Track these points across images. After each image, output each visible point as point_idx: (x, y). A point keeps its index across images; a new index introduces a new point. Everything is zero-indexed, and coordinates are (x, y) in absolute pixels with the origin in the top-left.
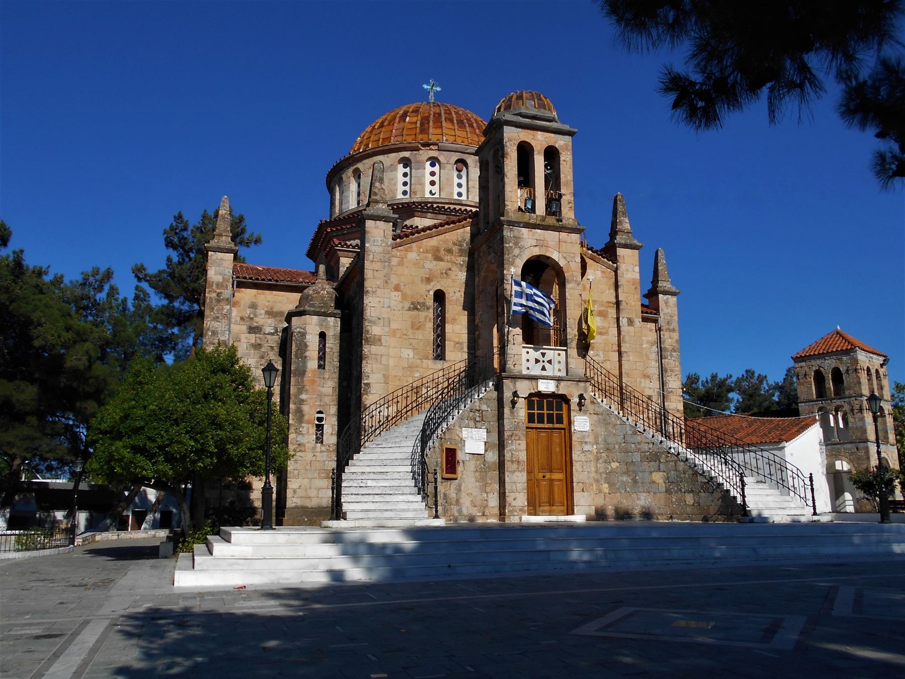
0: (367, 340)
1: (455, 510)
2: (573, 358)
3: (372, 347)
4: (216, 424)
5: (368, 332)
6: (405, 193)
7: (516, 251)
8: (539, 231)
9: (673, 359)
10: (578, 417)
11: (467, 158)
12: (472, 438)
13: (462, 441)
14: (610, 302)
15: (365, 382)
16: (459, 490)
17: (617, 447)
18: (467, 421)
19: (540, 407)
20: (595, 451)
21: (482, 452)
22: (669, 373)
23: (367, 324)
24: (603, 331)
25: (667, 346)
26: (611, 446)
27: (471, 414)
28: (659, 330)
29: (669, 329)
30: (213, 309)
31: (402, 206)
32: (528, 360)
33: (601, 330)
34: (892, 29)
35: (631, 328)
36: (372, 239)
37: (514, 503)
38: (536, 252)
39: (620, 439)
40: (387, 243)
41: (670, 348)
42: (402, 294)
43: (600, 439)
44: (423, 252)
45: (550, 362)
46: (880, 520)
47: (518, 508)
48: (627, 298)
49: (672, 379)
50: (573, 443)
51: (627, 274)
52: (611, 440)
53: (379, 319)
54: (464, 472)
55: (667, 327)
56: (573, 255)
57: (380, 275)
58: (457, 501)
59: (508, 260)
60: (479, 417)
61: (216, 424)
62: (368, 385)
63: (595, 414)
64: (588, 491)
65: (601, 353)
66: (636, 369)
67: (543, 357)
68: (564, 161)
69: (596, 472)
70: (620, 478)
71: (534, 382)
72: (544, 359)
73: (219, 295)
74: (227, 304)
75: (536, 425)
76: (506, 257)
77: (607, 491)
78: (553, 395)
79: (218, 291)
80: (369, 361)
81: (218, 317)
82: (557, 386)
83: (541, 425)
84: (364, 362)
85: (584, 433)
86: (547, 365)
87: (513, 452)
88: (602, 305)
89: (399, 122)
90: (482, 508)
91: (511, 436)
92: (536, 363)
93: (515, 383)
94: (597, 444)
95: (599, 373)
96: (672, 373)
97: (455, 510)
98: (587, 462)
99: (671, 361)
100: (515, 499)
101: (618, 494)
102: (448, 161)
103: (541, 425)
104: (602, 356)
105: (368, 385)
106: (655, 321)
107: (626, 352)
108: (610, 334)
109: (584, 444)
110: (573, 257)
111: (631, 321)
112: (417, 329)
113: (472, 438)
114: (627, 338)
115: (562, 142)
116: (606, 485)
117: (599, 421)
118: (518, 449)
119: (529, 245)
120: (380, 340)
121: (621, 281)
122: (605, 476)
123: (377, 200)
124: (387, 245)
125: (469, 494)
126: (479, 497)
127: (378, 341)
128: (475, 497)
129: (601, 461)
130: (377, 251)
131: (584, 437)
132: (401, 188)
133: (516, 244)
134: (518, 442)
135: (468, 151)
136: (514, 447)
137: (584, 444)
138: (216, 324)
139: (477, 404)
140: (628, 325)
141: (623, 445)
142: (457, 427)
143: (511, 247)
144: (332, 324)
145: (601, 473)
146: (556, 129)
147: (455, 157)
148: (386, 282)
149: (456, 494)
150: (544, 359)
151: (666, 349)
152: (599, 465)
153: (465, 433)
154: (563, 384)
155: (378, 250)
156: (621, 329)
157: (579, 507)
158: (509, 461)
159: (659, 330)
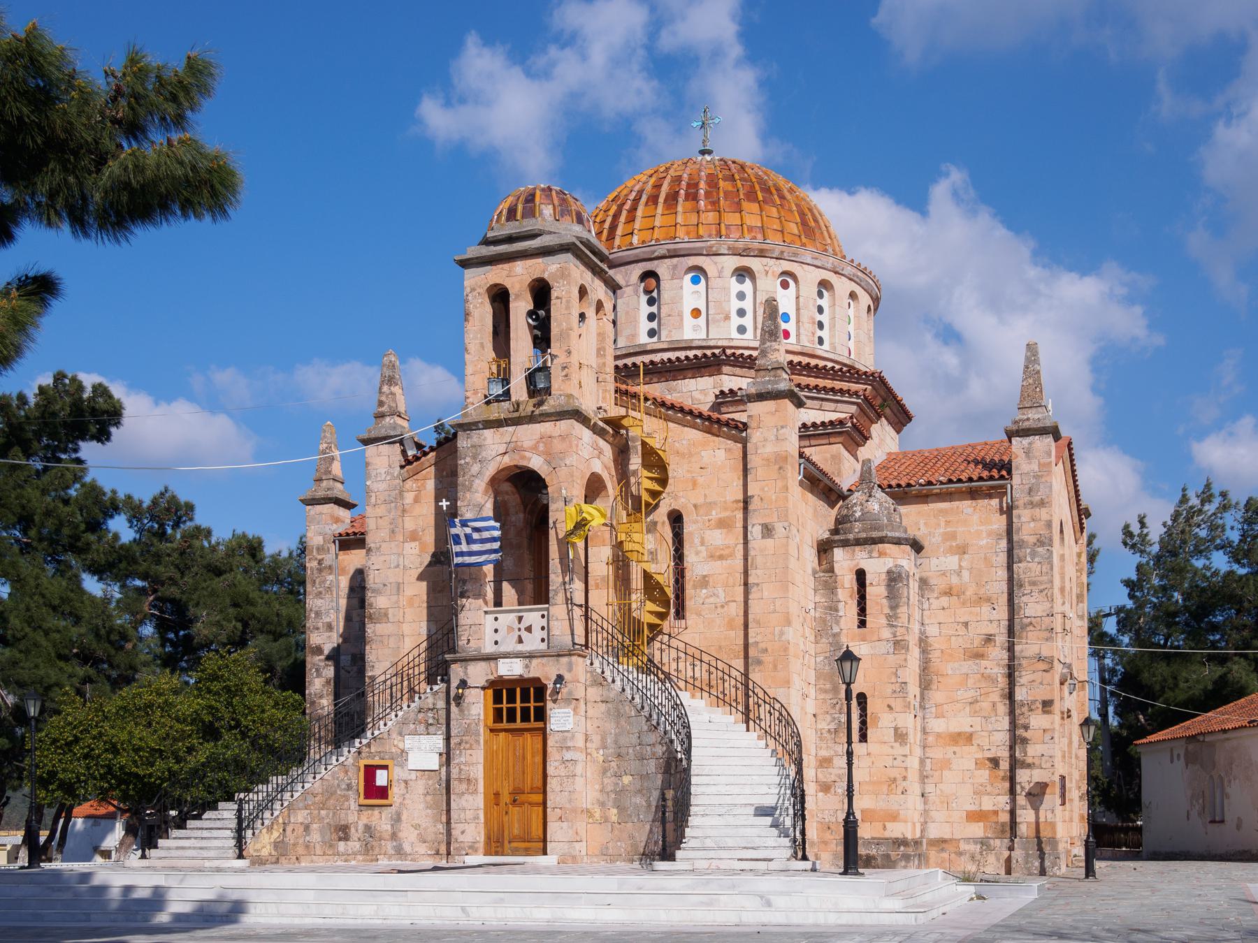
0: (370, 617)
1: (389, 848)
2: (557, 619)
3: (377, 625)
5: (371, 605)
6: (652, 333)
7: (475, 468)
9: (1036, 560)
10: (556, 711)
11: (657, 266)
12: (419, 749)
15: (370, 674)
16: (397, 819)
17: (631, 751)
18: (412, 726)
19: (511, 699)
20: (601, 759)
22: (1027, 589)
23: (369, 594)
24: (726, 552)
25: (1026, 538)
26: (623, 751)
27: (421, 716)
28: (1008, 511)
30: (314, 582)
32: (496, 631)
33: (722, 552)
34: (179, 213)
35: (769, 542)
36: (373, 474)
37: (461, 838)
38: (507, 461)
39: (634, 740)
40: (392, 474)
41: (1032, 539)
42: (420, 543)
43: (609, 741)
44: (447, 476)
45: (529, 629)
46: (842, 870)
47: (466, 844)
48: (763, 489)
49: (1032, 599)
50: (549, 749)
51: (763, 446)
52: (624, 741)
53: (385, 585)
54: (407, 796)
55: (1027, 498)
57: (384, 523)
58: (394, 836)
59: (463, 485)
60: (434, 718)
62: (373, 678)
63: (602, 702)
64: (568, 821)
65: (720, 591)
66: (774, 611)
68: (557, 298)
69: (601, 791)
70: (633, 800)
71: (492, 663)
73: (320, 562)
74: (330, 574)
75: (505, 725)
76: (460, 479)
77: (614, 819)
78: (521, 681)
79: (320, 557)
80: (374, 647)
81: (320, 593)
82: (527, 667)
83: (512, 726)
84: (367, 647)
85: (566, 734)
86: (524, 634)
87: (462, 767)
88: (726, 509)
89: (646, 204)
90: (436, 844)
91: (460, 744)
93: (466, 668)
94: (604, 747)
95: (610, 637)
96: (1033, 588)
97: (389, 848)
98: (568, 777)
99: (1034, 566)
100: (463, 832)
101: (630, 825)
102: (627, 282)
103: (512, 726)
104: (722, 595)
105: (373, 678)
107: (758, 584)
109: (564, 750)
111: (768, 530)
112: (439, 592)
113: (419, 749)
114: (759, 560)
115: (555, 266)
116: (615, 811)
117: (608, 711)
118: (473, 762)
119: (494, 453)
120: (386, 615)
121: (753, 460)
122: (613, 796)
123: (382, 412)
124: (394, 478)
125: (417, 827)
126: (431, 830)
127: (383, 617)
128: (425, 829)
129: (609, 774)
130: (381, 489)
131: (565, 739)
132: (645, 325)
133: (474, 457)
134: (469, 752)
135: (656, 254)
136: (463, 759)
137: (564, 750)
138: (319, 602)
139: (430, 700)
141: (638, 748)
142: (394, 735)
143: (467, 463)
145: (608, 793)
146: (537, 248)
147: (638, 269)
148: (393, 532)
149: (392, 825)
151: (1022, 544)
152: (606, 781)
153: (409, 742)
154: (535, 662)
155: (382, 486)
156: (750, 546)
157: (553, 844)
158: (455, 779)
159: (1008, 511)
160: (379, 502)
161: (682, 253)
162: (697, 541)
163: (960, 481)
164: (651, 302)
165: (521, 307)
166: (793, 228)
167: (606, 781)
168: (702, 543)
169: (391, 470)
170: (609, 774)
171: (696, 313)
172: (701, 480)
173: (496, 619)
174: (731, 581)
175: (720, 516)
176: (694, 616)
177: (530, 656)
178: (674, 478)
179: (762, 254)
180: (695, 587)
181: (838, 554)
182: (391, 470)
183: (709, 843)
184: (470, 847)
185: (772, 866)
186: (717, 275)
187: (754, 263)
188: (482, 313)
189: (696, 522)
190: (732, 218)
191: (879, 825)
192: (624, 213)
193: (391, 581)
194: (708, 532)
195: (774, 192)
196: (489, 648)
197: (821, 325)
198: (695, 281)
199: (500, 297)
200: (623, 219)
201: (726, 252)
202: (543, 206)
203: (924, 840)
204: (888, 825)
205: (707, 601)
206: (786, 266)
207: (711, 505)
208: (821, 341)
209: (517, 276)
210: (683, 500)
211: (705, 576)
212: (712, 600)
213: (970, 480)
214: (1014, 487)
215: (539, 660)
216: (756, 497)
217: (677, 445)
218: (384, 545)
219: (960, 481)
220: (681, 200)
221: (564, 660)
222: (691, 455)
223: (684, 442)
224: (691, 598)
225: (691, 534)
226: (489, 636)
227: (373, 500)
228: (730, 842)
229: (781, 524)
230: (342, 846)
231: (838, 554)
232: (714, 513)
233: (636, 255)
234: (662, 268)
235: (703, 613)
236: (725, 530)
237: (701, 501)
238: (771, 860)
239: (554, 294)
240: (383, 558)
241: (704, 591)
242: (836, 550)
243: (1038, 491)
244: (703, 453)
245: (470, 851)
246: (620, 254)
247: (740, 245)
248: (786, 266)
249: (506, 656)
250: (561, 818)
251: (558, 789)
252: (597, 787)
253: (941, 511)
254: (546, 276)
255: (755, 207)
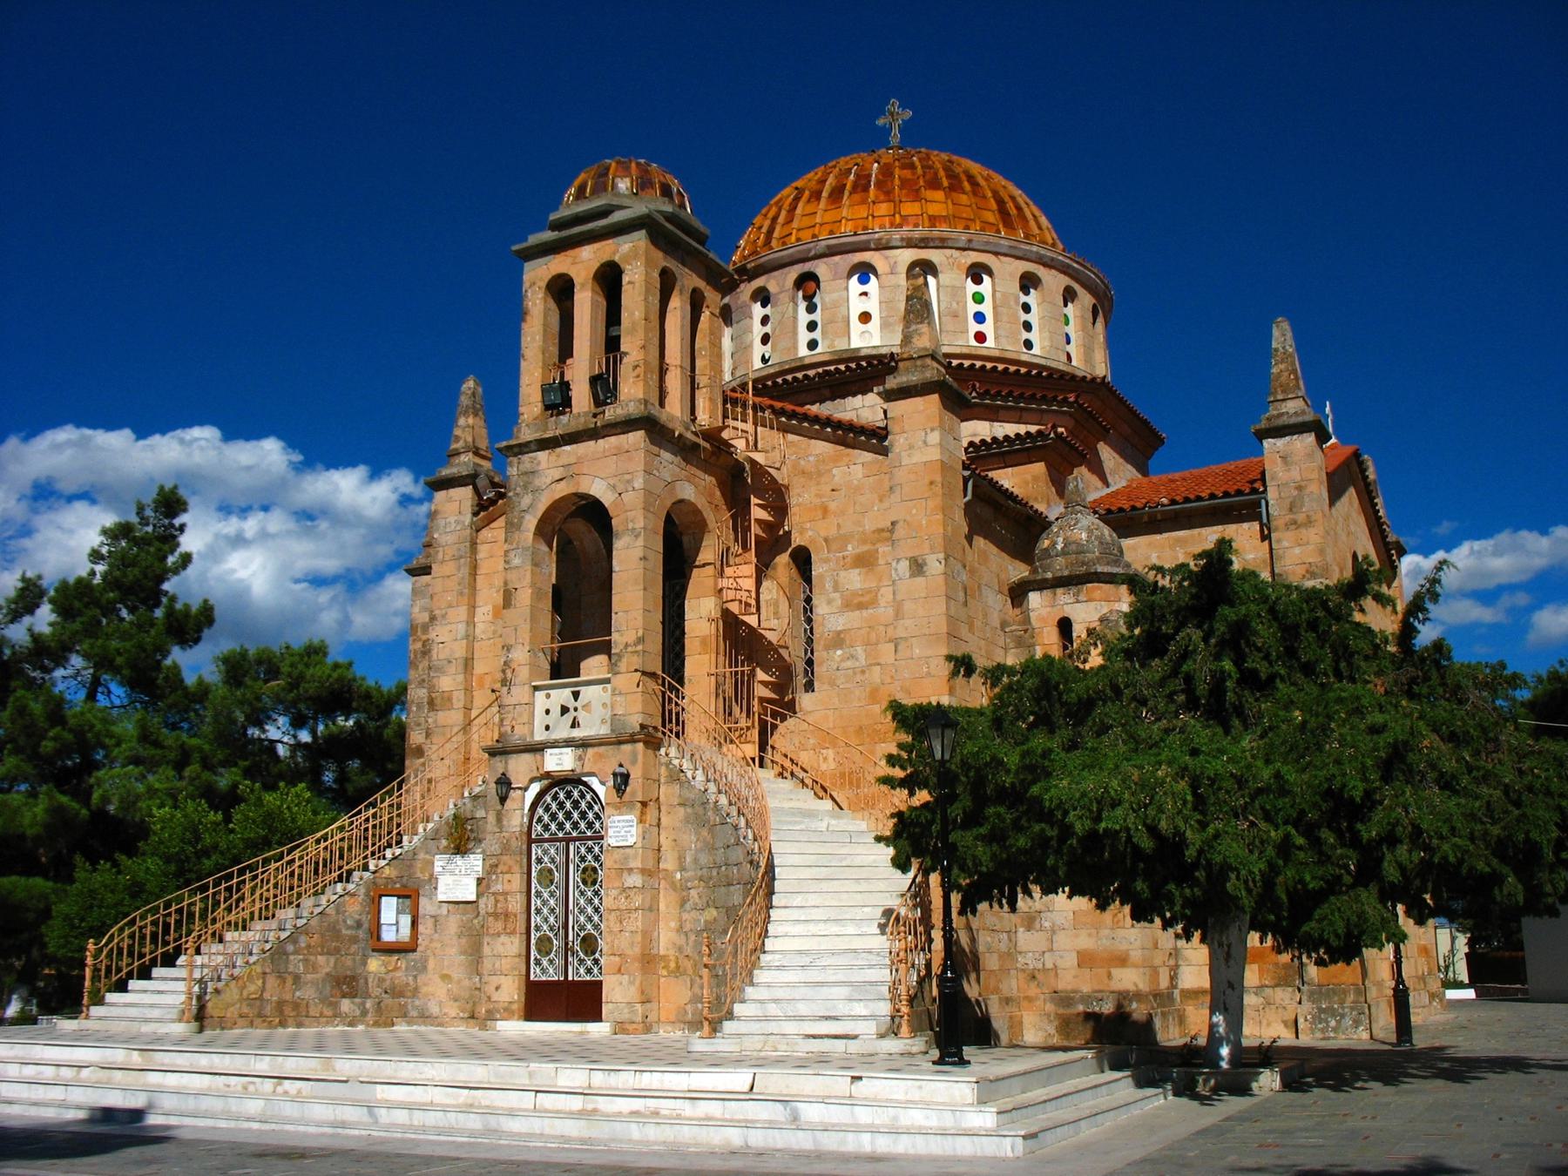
2: (620, 694)
4: (1321, 853)
6: (812, 345)
7: (526, 501)
8: (568, 448)
10: (617, 818)
13: (433, 880)
14: (883, 530)
21: (473, 897)
29: (1295, 522)
31: (869, 364)
32: (548, 712)
33: (861, 599)
38: (562, 490)
43: (688, 860)
47: (501, 1005)
53: (450, 662)
56: (627, 477)
61: (1321, 853)
65: (860, 650)
67: (576, 699)
68: (629, 283)
69: (678, 931)
71: (538, 756)
72: (576, 704)
82: (580, 758)
85: (628, 850)
86: (571, 704)
89: (809, 201)
92: (562, 715)
100: (497, 988)
106: (1258, 517)
108: (882, 602)
109: (625, 874)
110: (628, 482)
119: (549, 481)
120: (450, 699)
125: (446, 978)
126: (466, 983)
132: (804, 336)
134: (507, 876)
137: (625, 874)
140: (913, 575)
144: (1116, 606)
147: (793, 273)
150: (576, 704)
160: (447, 558)
161: (848, 248)
162: (829, 586)
163: (1199, 499)
164: (811, 309)
165: (586, 303)
166: (991, 217)
167: (685, 916)
168: (836, 588)
169: (462, 518)
170: (688, 906)
171: (865, 317)
172: (833, 506)
173: (548, 696)
174: (873, 636)
175: (858, 551)
176: (826, 687)
177: (583, 744)
178: (799, 505)
179: (942, 244)
180: (827, 648)
181: (1034, 598)
182: (462, 518)
183: (773, 1009)
184: (505, 1010)
185: (853, 1047)
186: (888, 270)
187: (934, 256)
188: (537, 304)
189: (827, 561)
190: (910, 208)
191: (1102, 972)
192: (783, 213)
193: (457, 656)
194: (842, 574)
195: (964, 178)
196: (540, 736)
197: (1028, 326)
198: (864, 280)
199: (562, 290)
200: (781, 220)
201: (899, 244)
202: (618, 180)
203: (1176, 992)
204: (1116, 972)
205: (844, 665)
206: (974, 257)
207: (845, 540)
208: (1028, 344)
209: (582, 263)
210: (810, 533)
211: (839, 633)
212: (849, 664)
213: (1212, 496)
214: (1271, 502)
215: (596, 749)
216: (901, 523)
217: (802, 462)
218: (450, 611)
219: (1199, 499)
220: (846, 193)
221: (627, 748)
222: (820, 474)
223: (811, 459)
224: (821, 664)
225: (821, 576)
226: (539, 719)
227: (440, 556)
228: (803, 1009)
229: (934, 557)
230: (346, 1005)
231: (1034, 598)
232: (850, 547)
233: (791, 255)
234: (821, 268)
235: (838, 682)
236: (864, 570)
237: (833, 532)
238: (855, 1037)
239: (625, 279)
240: (449, 627)
241: (839, 652)
242: (1031, 595)
243: (1302, 506)
244: (835, 471)
245: (505, 1014)
246: (771, 256)
247: (917, 235)
248: (974, 257)
249: (555, 744)
250: (619, 970)
251: (616, 928)
252: (673, 924)
253: (1178, 540)
254: (616, 259)
255: (939, 195)
